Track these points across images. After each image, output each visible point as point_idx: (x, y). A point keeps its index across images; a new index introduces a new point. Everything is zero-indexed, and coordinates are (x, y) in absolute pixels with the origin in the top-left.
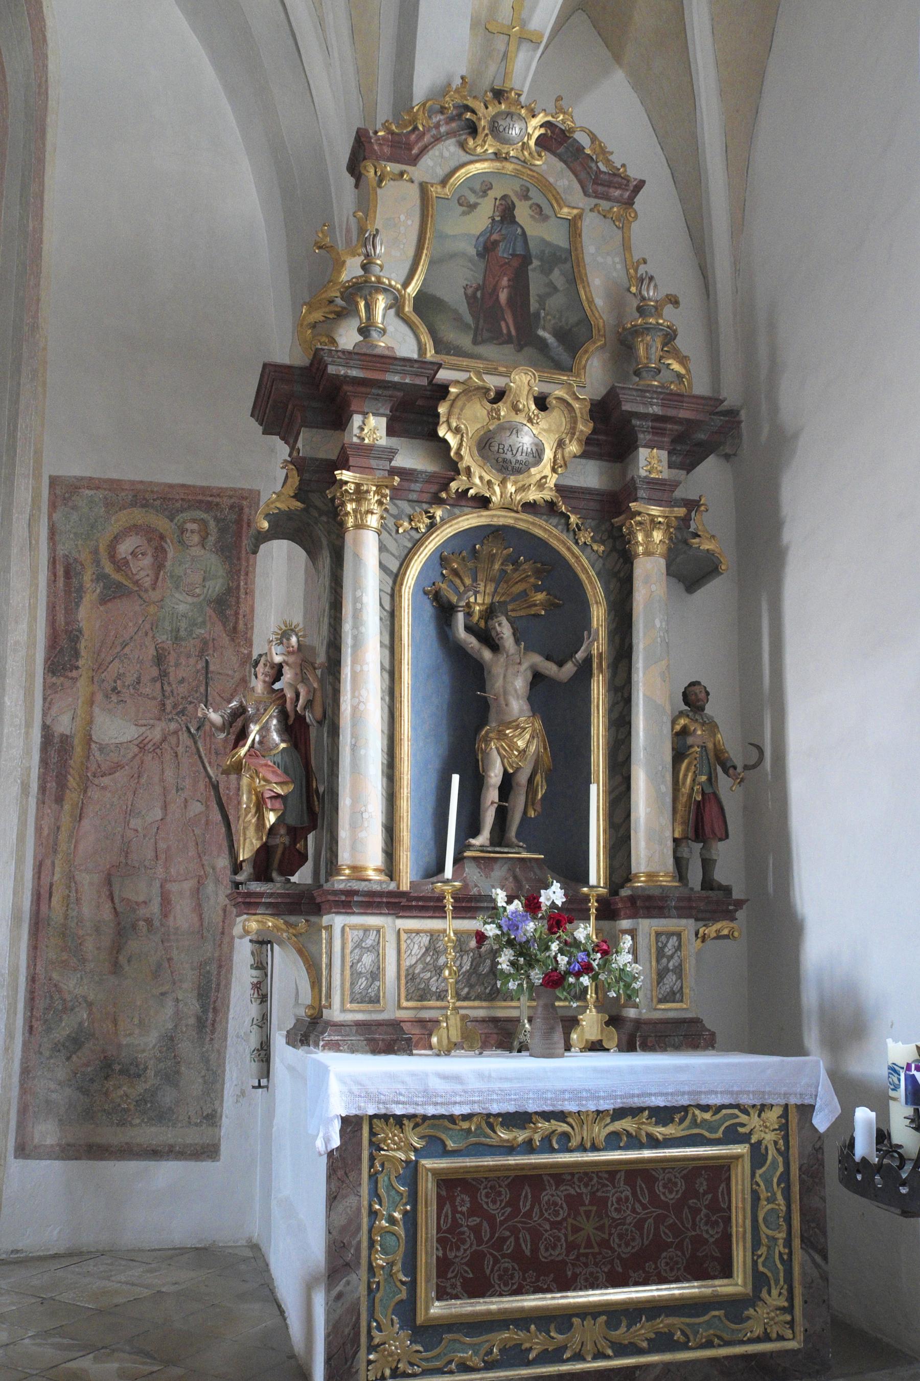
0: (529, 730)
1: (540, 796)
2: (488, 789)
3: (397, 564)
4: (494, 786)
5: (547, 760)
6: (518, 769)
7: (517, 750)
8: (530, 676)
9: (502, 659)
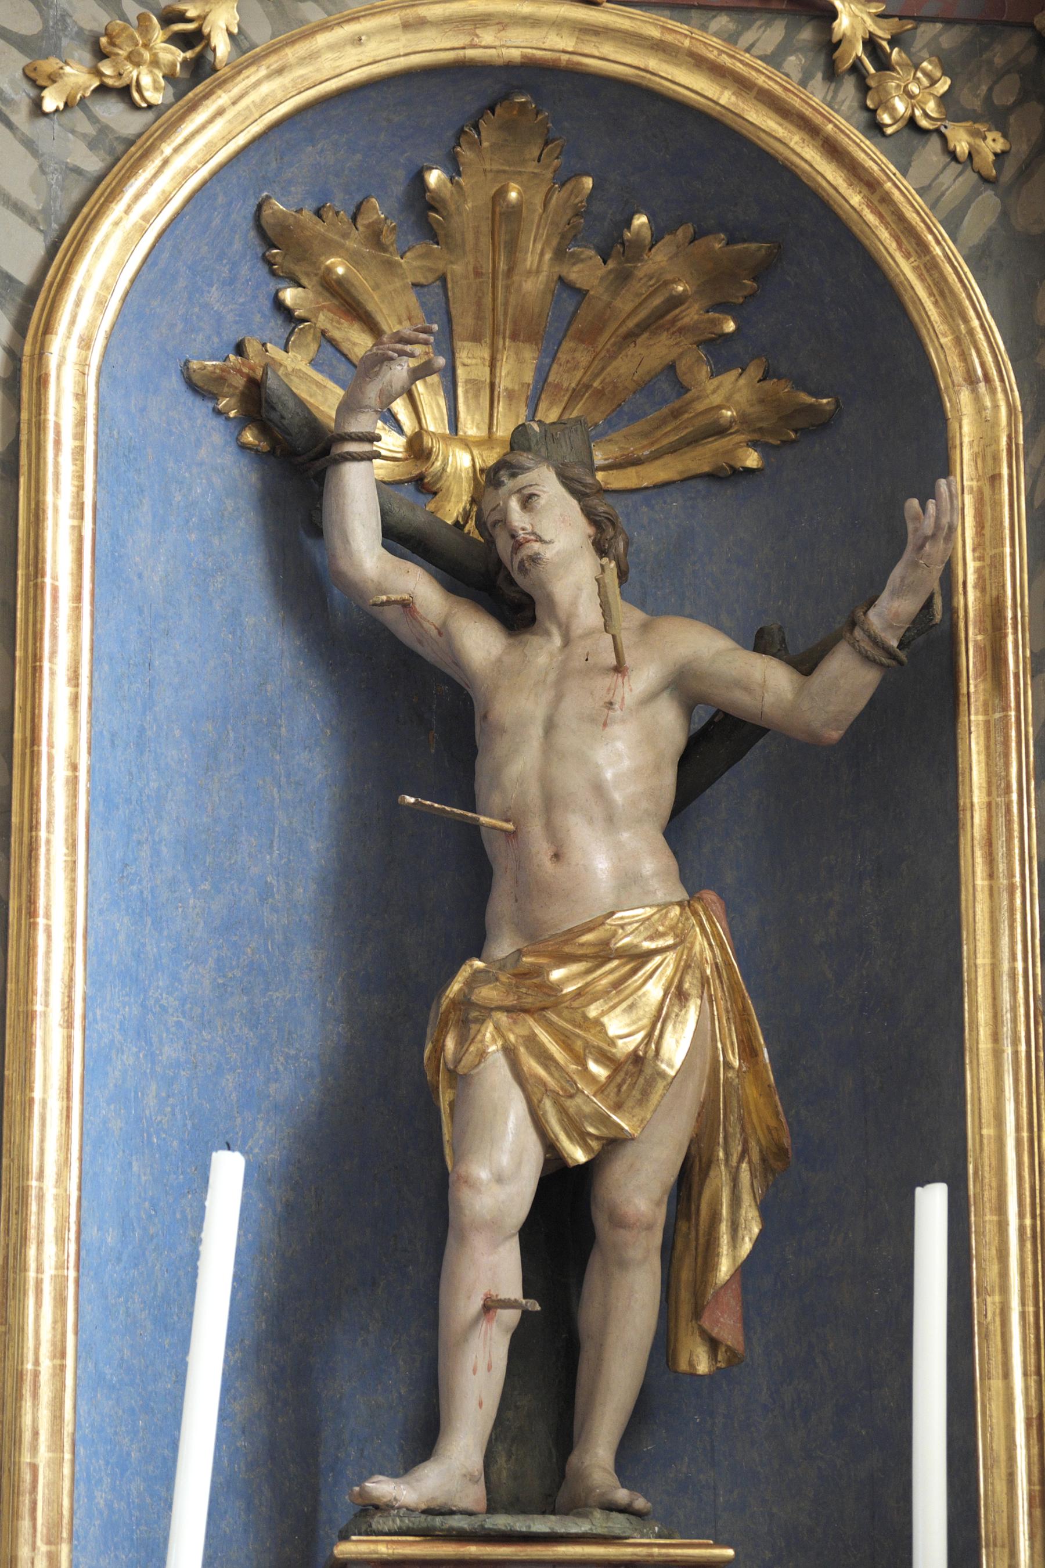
0: (666, 967)
1: (725, 1268)
2: (462, 1238)
3: (36, 246)
4: (493, 1225)
5: (760, 1105)
6: (613, 1144)
7: (605, 1057)
8: (670, 726)
9: (543, 651)
